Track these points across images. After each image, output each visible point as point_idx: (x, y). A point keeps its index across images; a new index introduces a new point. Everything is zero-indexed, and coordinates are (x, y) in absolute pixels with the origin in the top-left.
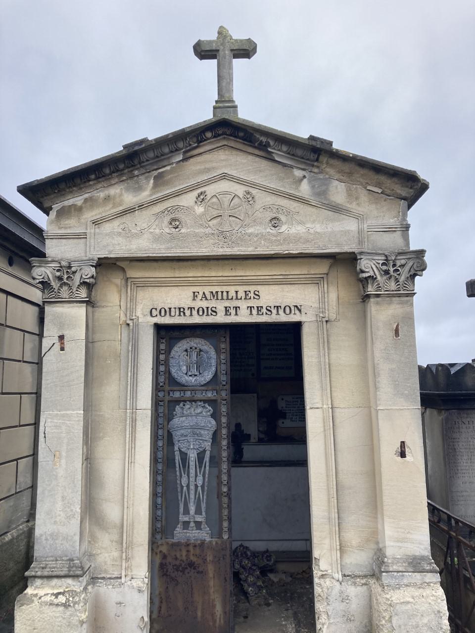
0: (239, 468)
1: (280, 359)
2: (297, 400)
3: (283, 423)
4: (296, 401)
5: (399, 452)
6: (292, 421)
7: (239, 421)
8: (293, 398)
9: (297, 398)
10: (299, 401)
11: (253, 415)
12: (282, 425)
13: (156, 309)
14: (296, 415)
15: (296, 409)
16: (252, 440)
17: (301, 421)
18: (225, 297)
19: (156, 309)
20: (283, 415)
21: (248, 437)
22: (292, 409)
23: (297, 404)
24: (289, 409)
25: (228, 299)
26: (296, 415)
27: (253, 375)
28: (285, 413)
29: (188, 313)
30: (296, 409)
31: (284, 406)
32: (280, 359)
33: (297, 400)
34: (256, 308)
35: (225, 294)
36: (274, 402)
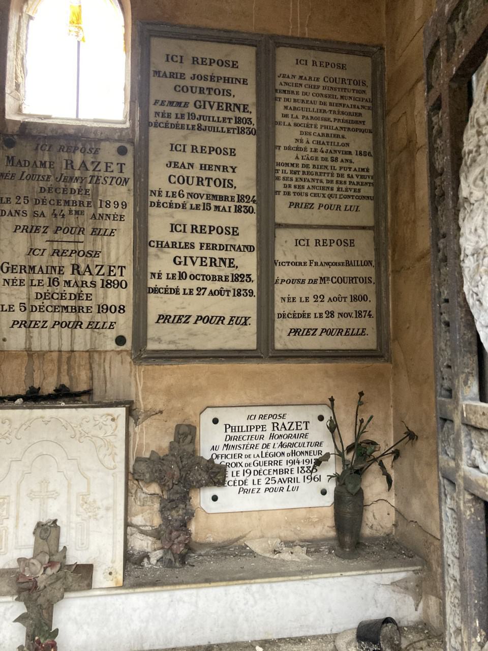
0: (60, 410)
1: (212, 293)
2: (261, 422)
3: (215, 498)
4: (257, 428)
5: (469, 501)
6: (246, 491)
7: (53, 511)
8: (249, 417)
9: (262, 417)
10: (269, 428)
11: (109, 485)
12: (212, 507)
13: (175, 176)
14: (259, 473)
15: (258, 451)
16: (100, 578)
17: (275, 490)
18: (240, 430)
19: (175, 176)
20: (216, 475)
21: (84, 574)
22: (244, 452)
23: (262, 437)
24: (237, 452)
25: (242, 431)
26: (259, 473)
27: (120, 340)
28: (222, 470)
29: (205, 183)
30: (258, 451)
31: (220, 440)
32: (212, 293)
33: (261, 422)
34: (234, 119)
35: (240, 428)
36: (187, 434)
